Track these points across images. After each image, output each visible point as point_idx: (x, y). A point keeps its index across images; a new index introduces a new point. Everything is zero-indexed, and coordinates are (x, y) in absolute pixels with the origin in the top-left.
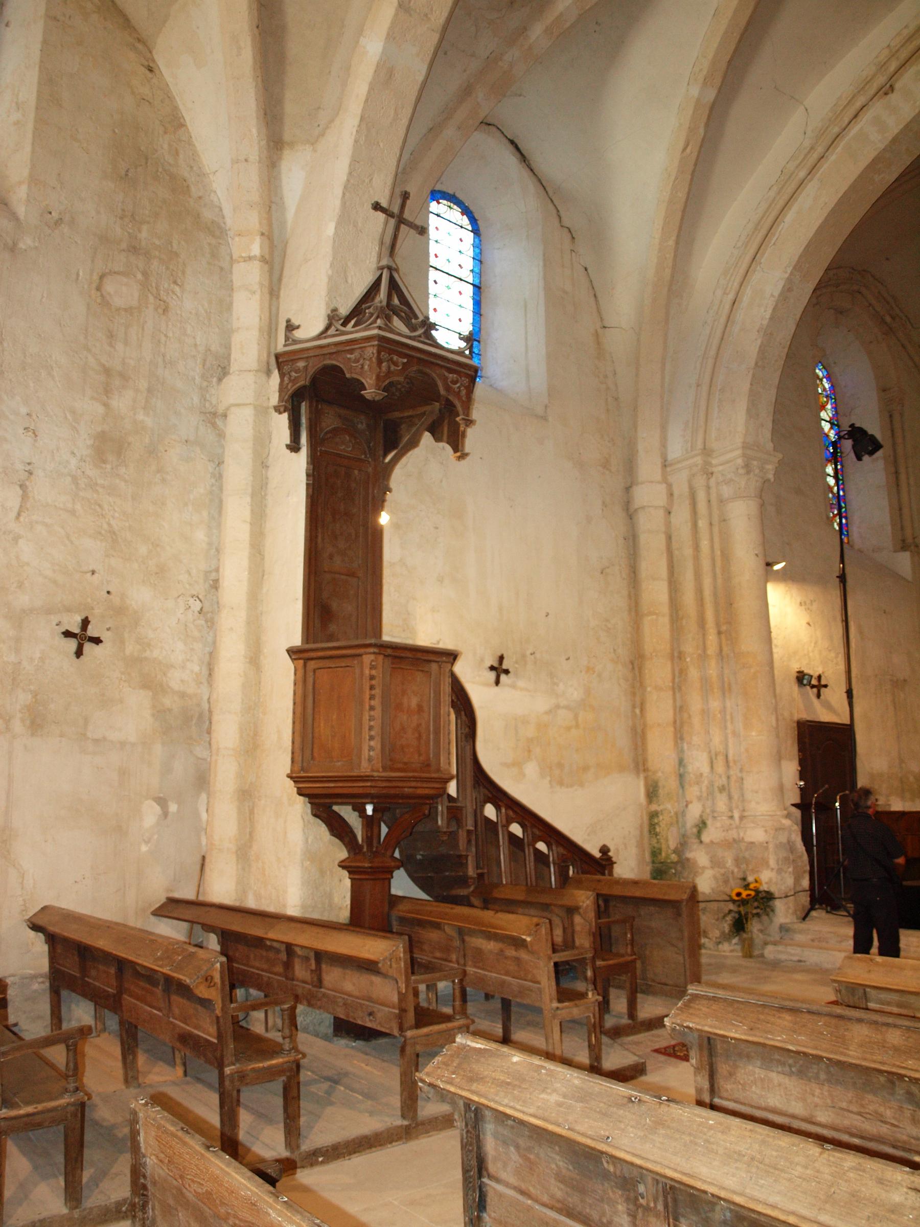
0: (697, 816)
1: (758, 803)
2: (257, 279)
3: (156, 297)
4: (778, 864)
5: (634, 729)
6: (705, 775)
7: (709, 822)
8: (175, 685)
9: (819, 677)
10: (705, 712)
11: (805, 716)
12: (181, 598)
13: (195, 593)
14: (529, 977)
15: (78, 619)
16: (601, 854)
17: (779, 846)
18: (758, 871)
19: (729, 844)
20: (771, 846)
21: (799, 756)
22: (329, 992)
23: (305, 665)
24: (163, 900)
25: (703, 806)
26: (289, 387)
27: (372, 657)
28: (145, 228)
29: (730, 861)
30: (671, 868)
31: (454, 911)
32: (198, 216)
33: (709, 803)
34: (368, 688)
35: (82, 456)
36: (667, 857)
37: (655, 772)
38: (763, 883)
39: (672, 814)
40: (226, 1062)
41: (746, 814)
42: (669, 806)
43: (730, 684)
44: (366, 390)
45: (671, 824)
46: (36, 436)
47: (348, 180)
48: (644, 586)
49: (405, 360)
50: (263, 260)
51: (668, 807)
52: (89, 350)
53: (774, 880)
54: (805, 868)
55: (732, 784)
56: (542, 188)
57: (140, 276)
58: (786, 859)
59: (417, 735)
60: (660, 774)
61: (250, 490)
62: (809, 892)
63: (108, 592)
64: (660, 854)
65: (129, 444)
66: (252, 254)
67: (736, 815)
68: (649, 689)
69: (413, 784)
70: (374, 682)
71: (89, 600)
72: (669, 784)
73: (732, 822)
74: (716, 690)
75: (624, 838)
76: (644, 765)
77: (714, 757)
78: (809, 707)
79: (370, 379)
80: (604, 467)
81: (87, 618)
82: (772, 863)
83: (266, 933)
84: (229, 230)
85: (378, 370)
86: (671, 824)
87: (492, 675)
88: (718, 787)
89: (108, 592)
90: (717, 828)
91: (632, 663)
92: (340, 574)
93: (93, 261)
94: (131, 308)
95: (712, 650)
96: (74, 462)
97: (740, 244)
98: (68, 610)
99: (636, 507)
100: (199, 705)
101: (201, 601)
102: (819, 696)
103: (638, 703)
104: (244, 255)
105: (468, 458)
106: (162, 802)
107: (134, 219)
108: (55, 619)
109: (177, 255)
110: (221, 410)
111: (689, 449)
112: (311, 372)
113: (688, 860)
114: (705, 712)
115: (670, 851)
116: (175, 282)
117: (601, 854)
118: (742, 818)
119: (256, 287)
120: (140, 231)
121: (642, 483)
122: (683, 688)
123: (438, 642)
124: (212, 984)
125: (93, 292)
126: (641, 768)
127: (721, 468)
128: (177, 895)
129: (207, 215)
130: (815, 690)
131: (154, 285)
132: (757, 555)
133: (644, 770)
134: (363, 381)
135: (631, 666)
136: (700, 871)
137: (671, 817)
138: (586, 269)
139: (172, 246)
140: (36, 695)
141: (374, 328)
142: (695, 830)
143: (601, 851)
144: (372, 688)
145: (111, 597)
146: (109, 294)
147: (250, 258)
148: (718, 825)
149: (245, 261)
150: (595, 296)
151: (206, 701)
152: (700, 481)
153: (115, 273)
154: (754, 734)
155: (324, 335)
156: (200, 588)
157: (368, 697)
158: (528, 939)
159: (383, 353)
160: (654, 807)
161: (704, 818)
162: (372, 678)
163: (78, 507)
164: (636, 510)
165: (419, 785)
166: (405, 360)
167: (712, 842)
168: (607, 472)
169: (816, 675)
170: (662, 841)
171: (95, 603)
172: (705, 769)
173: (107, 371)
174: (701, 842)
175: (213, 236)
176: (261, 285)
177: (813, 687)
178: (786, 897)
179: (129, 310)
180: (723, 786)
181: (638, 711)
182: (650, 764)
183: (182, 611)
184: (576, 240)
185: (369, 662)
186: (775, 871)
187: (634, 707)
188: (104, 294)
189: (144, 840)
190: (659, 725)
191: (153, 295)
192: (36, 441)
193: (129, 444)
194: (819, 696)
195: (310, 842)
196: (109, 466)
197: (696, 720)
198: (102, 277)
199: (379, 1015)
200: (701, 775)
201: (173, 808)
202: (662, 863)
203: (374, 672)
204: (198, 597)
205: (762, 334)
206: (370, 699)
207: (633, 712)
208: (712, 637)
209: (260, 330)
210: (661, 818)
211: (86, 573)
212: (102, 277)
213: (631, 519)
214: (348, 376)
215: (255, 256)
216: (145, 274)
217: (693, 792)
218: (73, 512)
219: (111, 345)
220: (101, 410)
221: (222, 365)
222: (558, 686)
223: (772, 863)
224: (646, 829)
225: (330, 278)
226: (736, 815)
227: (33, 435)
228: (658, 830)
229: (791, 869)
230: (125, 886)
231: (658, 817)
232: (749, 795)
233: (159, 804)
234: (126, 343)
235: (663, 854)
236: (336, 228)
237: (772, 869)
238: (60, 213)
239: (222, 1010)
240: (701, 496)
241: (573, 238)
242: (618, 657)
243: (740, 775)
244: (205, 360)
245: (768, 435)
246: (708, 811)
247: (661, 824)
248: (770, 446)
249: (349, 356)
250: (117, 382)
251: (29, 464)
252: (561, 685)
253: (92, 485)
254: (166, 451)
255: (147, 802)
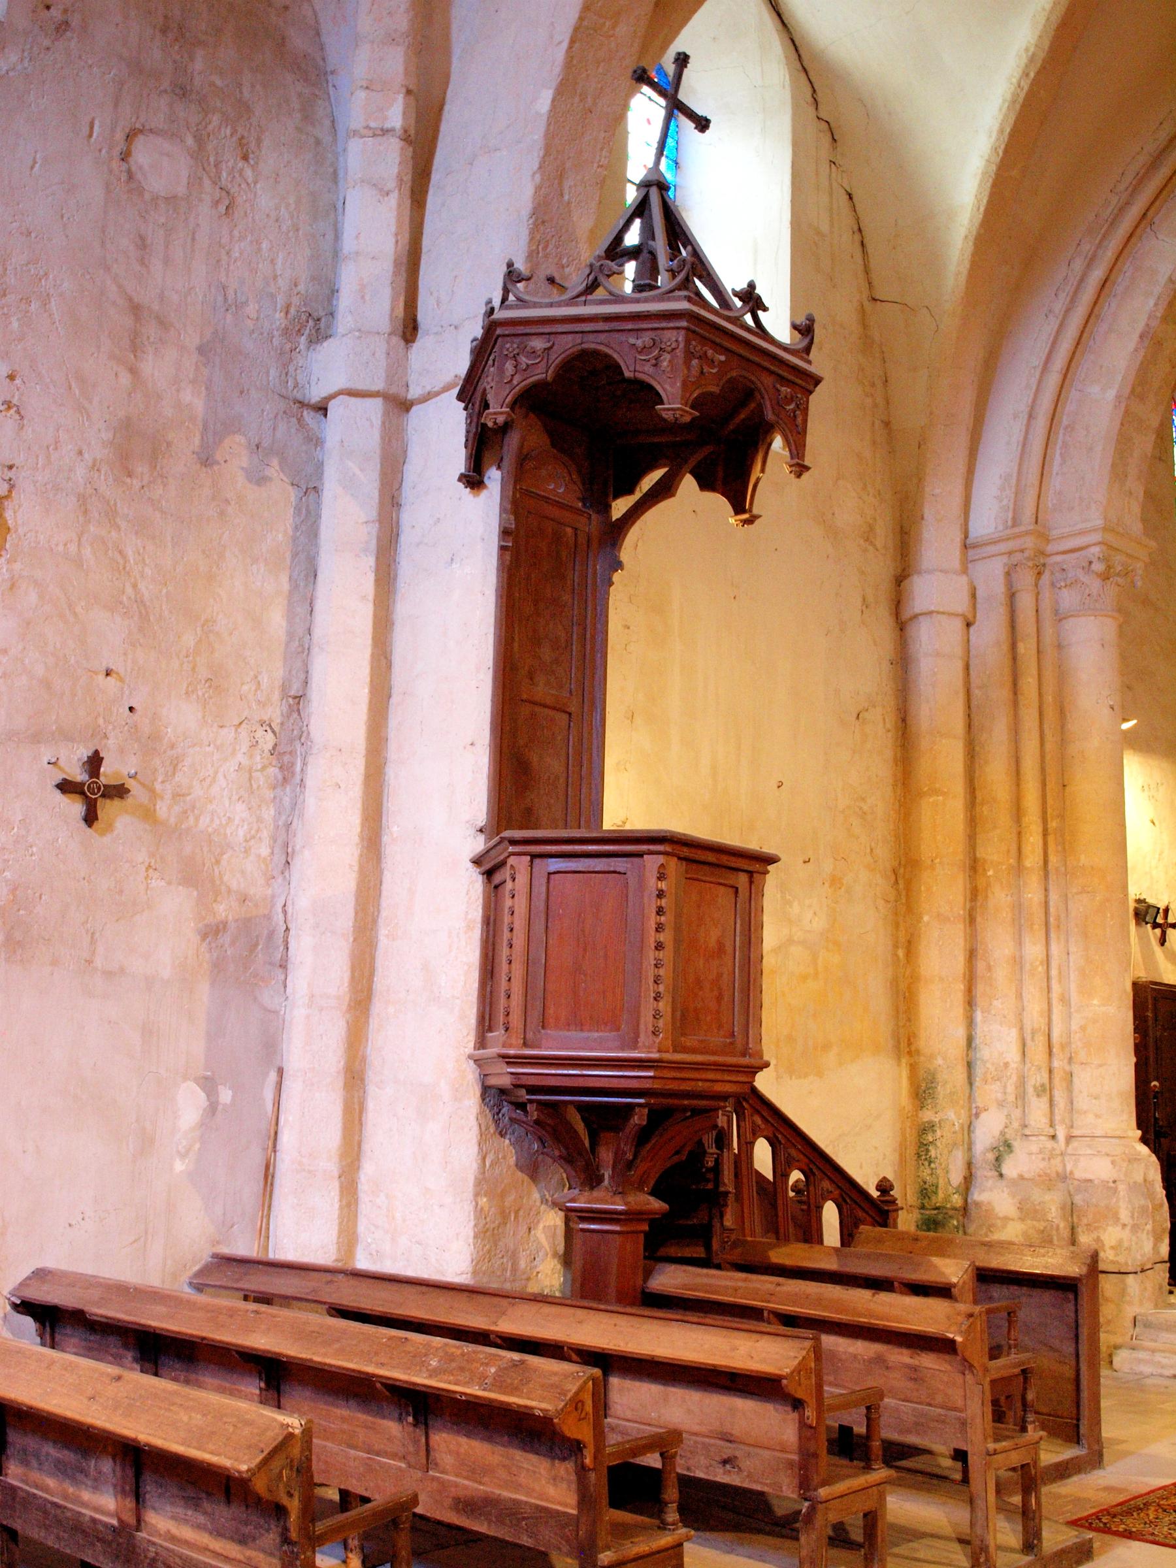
0: (997, 1133)
1: (1097, 1116)
2: (395, 170)
3: (215, 183)
4: (1132, 1217)
5: (894, 982)
6: (1013, 1065)
7: (1016, 1144)
8: (234, 882)
9: (1167, 910)
10: (1018, 962)
11: (1143, 975)
12: (244, 725)
13: (266, 718)
14: (939, 1399)
15: (85, 753)
16: (879, 1193)
17: (1133, 1187)
18: (1096, 1228)
19: (1049, 1181)
20: (1122, 1187)
21: (1135, 1038)
22: (628, 1424)
23: (531, 861)
24: (205, 1258)
25: (1008, 1116)
26: (515, 382)
27: (661, 859)
28: (200, 53)
29: (1053, 1210)
30: (951, 1217)
31: (785, 1288)
32: (283, 42)
33: (1017, 1113)
34: (654, 910)
35: (95, 461)
36: (947, 1198)
37: (932, 1057)
38: (1107, 1247)
39: (957, 1127)
40: (600, 1544)
41: (1076, 1132)
42: (951, 1115)
43: (1058, 918)
44: (662, 403)
45: (955, 1144)
46: (22, 418)
47: (581, 19)
48: (924, 744)
49: (723, 358)
50: (406, 138)
51: (949, 1116)
52: (108, 269)
53: (1126, 1244)
54: (1164, 1226)
55: (1057, 1081)
56: (792, 48)
57: (190, 141)
58: (1143, 1210)
59: (716, 993)
60: (940, 1061)
61: (373, 545)
62: (1168, 1265)
63: (131, 709)
64: (936, 1193)
65: (169, 444)
66: (388, 125)
67: (1061, 1134)
68: (926, 918)
69: (711, 1076)
70: (663, 902)
71: (101, 721)
72: (951, 1078)
73: (1055, 1145)
74: (1036, 927)
75: (877, 1165)
76: (910, 1044)
77: (1028, 1037)
78: (1148, 957)
79: (672, 385)
80: (867, 540)
81: (97, 752)
82: (1124, 1215)
83: (495, 1323)
84: (332, 73)
85: (686, 372)
86: (955, 1144)
87: (75, 808)
88: (1035, 1088)
89: (131, 709)
90: (1030, 1154)
91: (894, 871)
92: (545, 706)
93: (116, 105)
94: (175, 197)
95: (1032, 859)
96: (80, 473)
97: (1122, 187)
98: (67, 736)
99: (917, 610)
100: (268, 917)
101: (274, 732)
102: (1163, 941)
103: (902, 939)
104: (373, 125)
105: (757, 522)
106: (209, 1085)
107: (183, 36)
108: (47, 755)
109: (248, 109)
110: (315, 394)
111: (1010, 523)
112: (556, 358)
113: (977, 1204)
114: (1018, 962)
115: (951, 1190)
116: (245, 158)
117: (878, 1193)
118: (1070, 1138)
119: (391, 184)
120: (192, 59)
121: (930, 572)
122: (979, 919)
123: (624, 823)
124: (583, 1415)
125: (115, 164)
126: (903, 1045)
127: (1058, 558)
128: (226, 1250)
129: (298, 41)
130: (1158, 931)
131: (212, 159)
132: (1112, 708)
133: (910, 1053)
134: (658, 388)
135: (893, 878)
136: (999, 1223)
137: (954, 1133)
138: (850, 197)
139: (241, 93)
140: (15, 889)
141: (678, 299)
142: (991, 1156)
143: (879, 1188)
144: (660, 911)
145: (135, 717)
146: (141, 168)
147: (385, 132)
148: (1034, 1148)
149: (374, 135)
150: (862, 244)
151: (280, 910)
152: (1025, 579)
153: (151, 131)
154: (1095, 1002)
155: (583, 298)
156: (275, 712)
157: (652, 925)
158: (959, 1339)
159: (694, 343)
160: (927, 1115)
161: (1008, 1136)
162: (661, 894)
163: (87, 552)
164: (915, 617)
165: (718, 1076)
166: (723, 358)
167: (1021, 1177)
168: (871, 548)
169: (1162, 906)
170: (939, 1171)
171: (110, 727)
172: (1012, 1055)
173: (136, 309)
174: (1001, 1175)
175: (306, 80)
176: (401, 181)
177: (1155, 925)
178: (1143, 1271)
179: (171, 200)
180: (1043, 1085)
181: (901, 953)
182: (922, 1043)
183: (244, 748)
184: (838, 143)
185: (656, 867)
186: (1129, 1228)
187: (896, 946)
188: (133, 169)
189: (178, 1152)
190: (941, 979)
191: (210, 177)
192: (22, 427)
193: (169, 444)
194: (1163, 941)
195: (488, 1164)
196: (136, 483)
197: (1001, 973)
198: (130, 137)
199: (746, 1464)
200: (1006, 1065)
201: (225, 1095)
202: (937, 1208)
203: (663, 885)
204: (270, 726)
205: (1146, 343)
206: (657, 930)
207: (895, 955)
208: (1033, 839)
209: (397, 264)
210: (939, 1133)
211: (96, 673)
212: (130, 137)
213: (901, 630)
214: (627, 374)
215: (392, 130)
216: (200, 141)
217: (988, 1092)
218: (78, 562)
219: (142, 262)
220: (125, 379)
221: (315, 315)
222: (791, 907)
223: (1124, 1215)
224: (911, 1151)
225: (538, 189)
226: (1061, 1134)
227: (17, 417)
228: (933, 1153)
229: (1149, 1227)
230: (146, 1233)
231: (934, 1132)
232: (1082, 1102)
233: (204, 1089)
234: (167, 261)
235: (941, 1195)
236: (553, 101)
237: (1124, 1225)
238: (65, 11)
239: (595, 1458)
240: (1026, 602)
241: (834, 140)
242: (876, 862)
243: (1067, 1068)
244: (288, 306)
245: (1136, 509)
246: (1016, 1125)
247: (938, 1143)
248: (1137, 528)
249: (632, 341)
250: (151, 330)
251: (11, 467)
252: (796, 904)
253: (111, 514)
254: (225, 461)
255: (185, 1085)
